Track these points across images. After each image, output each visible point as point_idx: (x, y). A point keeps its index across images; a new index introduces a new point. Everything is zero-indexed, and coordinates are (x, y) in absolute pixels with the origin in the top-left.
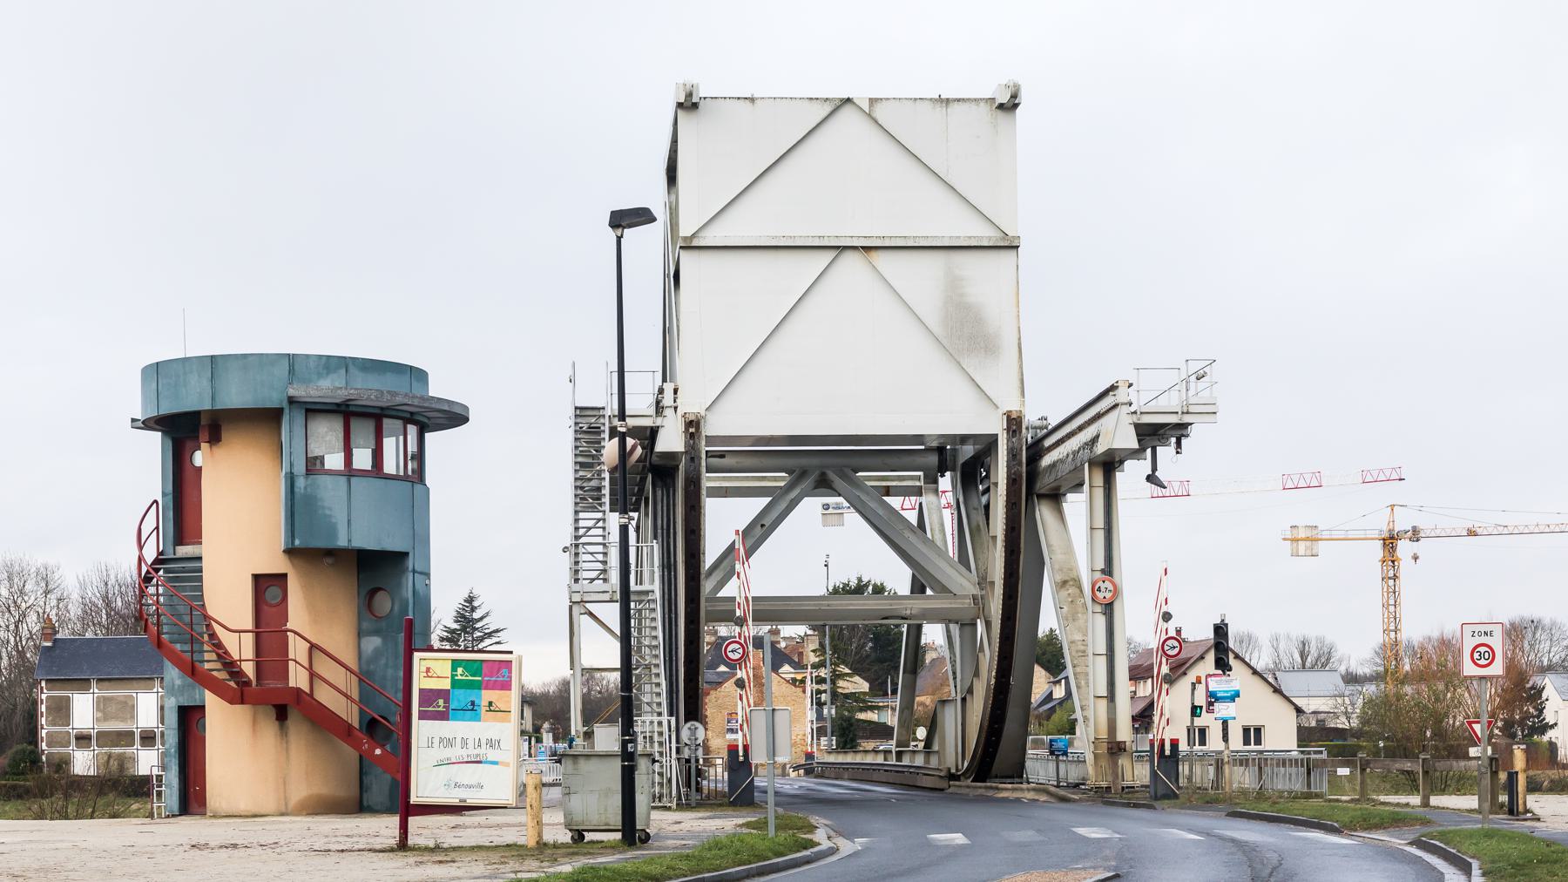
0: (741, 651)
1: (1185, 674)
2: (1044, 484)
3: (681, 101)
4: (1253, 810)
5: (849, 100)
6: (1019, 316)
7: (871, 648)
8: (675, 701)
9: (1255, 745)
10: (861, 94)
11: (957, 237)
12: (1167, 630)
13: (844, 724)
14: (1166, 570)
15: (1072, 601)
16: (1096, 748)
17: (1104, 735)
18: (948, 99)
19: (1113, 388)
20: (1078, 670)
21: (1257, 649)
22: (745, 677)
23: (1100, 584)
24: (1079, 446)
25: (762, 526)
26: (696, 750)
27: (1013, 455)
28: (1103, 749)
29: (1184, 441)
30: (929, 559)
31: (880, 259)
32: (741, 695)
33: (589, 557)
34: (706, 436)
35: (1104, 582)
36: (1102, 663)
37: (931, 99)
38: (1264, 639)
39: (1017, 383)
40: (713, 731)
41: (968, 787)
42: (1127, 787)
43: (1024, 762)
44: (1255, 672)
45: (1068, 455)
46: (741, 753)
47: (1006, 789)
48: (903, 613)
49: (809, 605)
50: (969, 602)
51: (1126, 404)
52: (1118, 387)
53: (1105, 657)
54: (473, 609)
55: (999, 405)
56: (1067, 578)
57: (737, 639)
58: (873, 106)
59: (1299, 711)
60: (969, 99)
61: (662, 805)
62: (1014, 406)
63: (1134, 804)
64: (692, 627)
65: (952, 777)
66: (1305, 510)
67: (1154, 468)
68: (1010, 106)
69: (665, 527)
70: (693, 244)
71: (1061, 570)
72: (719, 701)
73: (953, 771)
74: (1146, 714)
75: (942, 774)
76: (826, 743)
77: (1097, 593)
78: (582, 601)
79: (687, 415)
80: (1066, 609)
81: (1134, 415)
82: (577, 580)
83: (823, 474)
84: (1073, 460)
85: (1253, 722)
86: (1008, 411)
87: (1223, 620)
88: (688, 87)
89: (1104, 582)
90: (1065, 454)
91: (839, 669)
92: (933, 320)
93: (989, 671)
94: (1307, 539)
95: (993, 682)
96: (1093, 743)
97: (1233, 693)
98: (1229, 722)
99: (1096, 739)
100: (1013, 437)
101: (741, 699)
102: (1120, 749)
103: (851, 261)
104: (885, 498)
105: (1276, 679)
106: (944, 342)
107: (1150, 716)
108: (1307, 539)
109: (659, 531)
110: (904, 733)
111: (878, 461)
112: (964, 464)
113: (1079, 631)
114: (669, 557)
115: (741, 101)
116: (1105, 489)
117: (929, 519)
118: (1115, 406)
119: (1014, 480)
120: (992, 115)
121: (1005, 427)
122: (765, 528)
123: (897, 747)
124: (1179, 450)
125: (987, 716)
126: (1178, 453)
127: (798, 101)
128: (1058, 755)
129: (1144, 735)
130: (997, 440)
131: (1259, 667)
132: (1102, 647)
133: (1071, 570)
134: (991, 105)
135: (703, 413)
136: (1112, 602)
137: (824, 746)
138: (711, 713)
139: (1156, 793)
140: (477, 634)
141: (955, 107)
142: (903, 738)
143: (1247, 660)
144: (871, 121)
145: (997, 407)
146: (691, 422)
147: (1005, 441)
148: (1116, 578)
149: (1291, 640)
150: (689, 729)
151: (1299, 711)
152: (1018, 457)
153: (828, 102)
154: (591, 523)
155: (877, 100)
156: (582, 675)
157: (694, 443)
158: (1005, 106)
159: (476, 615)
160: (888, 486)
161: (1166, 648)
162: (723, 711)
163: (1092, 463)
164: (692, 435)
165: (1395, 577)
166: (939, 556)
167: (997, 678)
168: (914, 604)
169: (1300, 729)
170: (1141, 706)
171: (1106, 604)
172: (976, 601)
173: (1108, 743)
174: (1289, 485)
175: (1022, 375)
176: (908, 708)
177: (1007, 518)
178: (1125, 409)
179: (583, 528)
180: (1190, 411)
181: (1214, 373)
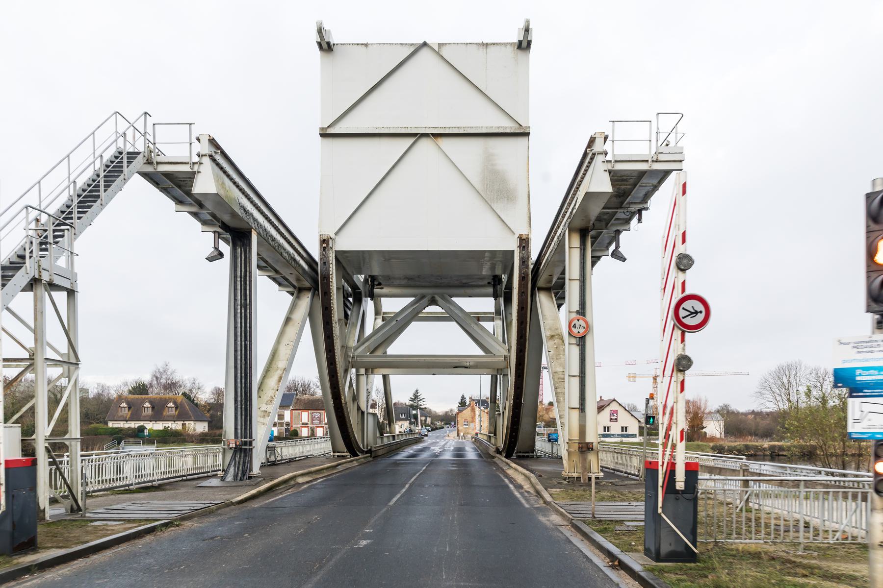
1: (603, 410)
5: (425, 44)
6: (528, 177)
12: (683, 283)
15: (556, 348)
16: (569, 447)
17: (576, 436)
18: (487, 43)
20: (558, 390)
23: (576, 322)
27: (523, 262)
28: (575, 448)
30: (485, 339)
31: (444, 143)
35: (578, 320)
36: (576, 382)
37: (477, 43)
39: (527, 219)
43: (534, 442)
50: (502, 359)
52: (595, 138)
53: (579, 249)
54: (417, 393)
55: (515, 232)
56: (554, 334)
58: (440, 48)
59: (639, 421)
62: (524, 231)
64: (332, 367)
66: (632, 370)
68: (524, 45)
69: (243, 276)
71: (550, 329)
77: (573, 329)
79: (322, 236)
80: (552, 352)
81: (609, 164)
83: (433, 297)
85: (624, 425)
86: (520, 235)
89: (578, 320)
94: (633, 377)
95: (512, 402)
96: (567, 443)
99: (569, 440)
100: (523, 250)
108: (633, 377)
109: (239, 279)
113: (560, 366)
114: (245, 299)
115: (360, 46)
119: (523, 278)
121: (518, 245)
125: (510, 421)
127: (394, 46)
128: (552, 442)
132: (576, 371)
133: (557, 329)
135: (333, 236)
136: (585, 336)
140: (418, 399)
141: (491, 49)
145: (514, 234)
146: (324, 240)
148: (588, 318)
151: (639, 421)
152: (526, 263)
153: (413, 46)
159: (418, 395)
160: (479, 317)
161: (682, 313)
165: (656, 387)
169: (640, 427)
171: (579, 338)
173: (579, 443)
175: (530, 214)
177: (519, 303)
178: (599, 159)
180: (660, 159)
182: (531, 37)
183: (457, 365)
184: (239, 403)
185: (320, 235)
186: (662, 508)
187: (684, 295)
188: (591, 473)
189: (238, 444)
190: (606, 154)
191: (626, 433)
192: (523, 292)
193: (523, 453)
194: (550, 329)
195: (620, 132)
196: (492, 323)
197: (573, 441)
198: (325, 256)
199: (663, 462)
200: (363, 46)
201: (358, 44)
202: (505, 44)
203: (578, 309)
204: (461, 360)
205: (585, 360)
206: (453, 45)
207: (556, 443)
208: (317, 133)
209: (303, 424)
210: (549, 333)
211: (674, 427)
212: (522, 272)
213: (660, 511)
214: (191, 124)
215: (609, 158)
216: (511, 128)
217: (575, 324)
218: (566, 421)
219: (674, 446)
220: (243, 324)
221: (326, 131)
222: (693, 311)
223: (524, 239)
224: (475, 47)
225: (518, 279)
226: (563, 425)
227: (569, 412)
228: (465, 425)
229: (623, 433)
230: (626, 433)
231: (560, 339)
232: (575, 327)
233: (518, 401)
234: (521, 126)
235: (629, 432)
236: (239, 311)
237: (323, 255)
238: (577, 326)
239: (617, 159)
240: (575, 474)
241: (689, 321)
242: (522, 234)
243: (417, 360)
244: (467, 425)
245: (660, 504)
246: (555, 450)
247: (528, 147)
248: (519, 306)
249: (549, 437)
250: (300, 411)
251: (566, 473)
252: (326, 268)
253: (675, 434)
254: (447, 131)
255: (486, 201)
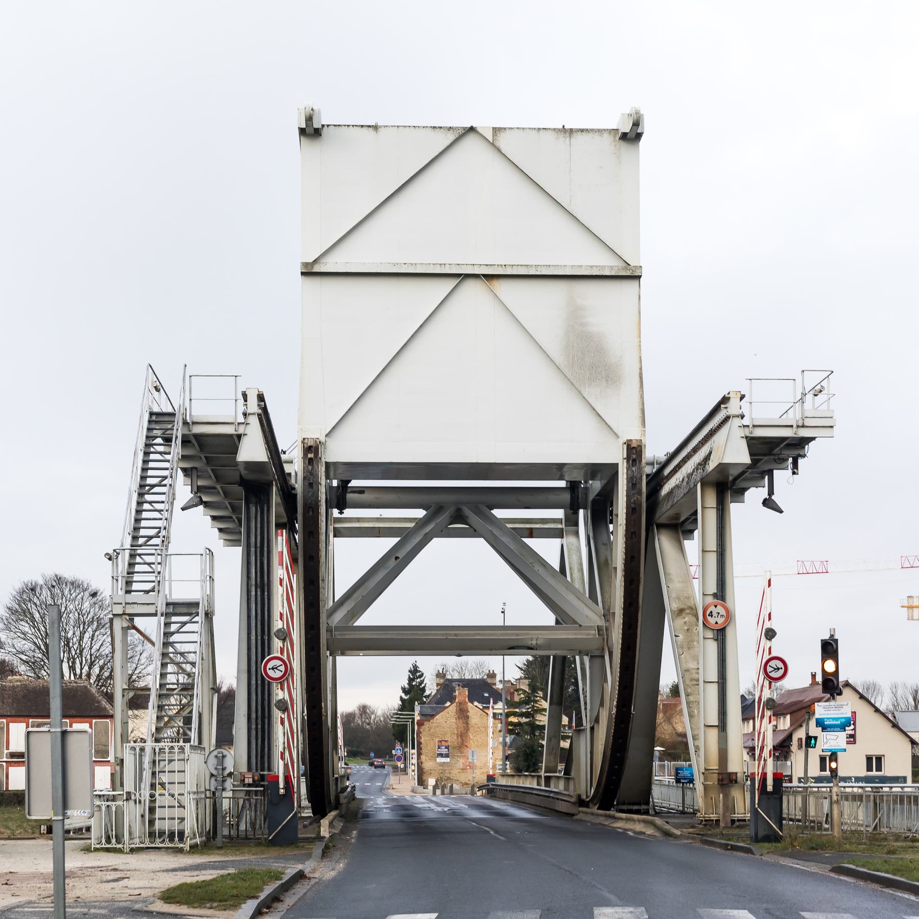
0: (282, 668)
2: (664, 513)
3: (304, 126)
4: (863, 866)
5: (472, 129)
6: (640, 346)
7: (573, 690)
8: (266, 727)
9: (876, 771)
10: (484, 124)
11: (579, 266)
12: (770, 649)
13: (527, 750)
14: (769, 581)
15: (688, 630)
16: (706, 779)
17: (714, 766)
18: (571, 130)
19: (725, 400)
20: (691, 698)
21: (880, 695)
22: (287, 697)
23: (712, 608)
24: (693, 467)
25: (397, 558)
26: (224, 781)
28: (713, 780)
29: (801, 461)
31: (504, 289)
32: (282, 719)
33: (146, 568)
34: (326, 463)
35: (716, 606)
36: (713, 690)
37: (555, 129)
38: (885, 685)
39: (638, 413)
40: (426, 755)
41: (592, 814)
42: (738, 820)
44: (877, 710)
45: (683, 479)
46: (281, 785)
47: (621, 819)
48: (529, 643)
49: (437, 634)
51: (738, 416)
52: (729, 398)
55: (619, 434)
57: (279, 655)
60: (592, 130)
61: (173, 845)
62: (634, 435)
63: (732, 846)
64: (312, 653)
65: (581, 803)
67: (771, 492)
69: (259, 545)
70: (314, 270)
71: (678, 598)
72: (432, 730)
73: (584, 797)
74: (785, 744)
75: (573, 800)
76: (501, 767)
77: (709, 618)
78: (124, 614)
79: (306, 441)
80: (681, 637)
81: (746, 429)
82: (128, 592)
83: (459, 510)
84: (687, 483)
87: (832, 636)
88: (309, 110)
89: (716, 606)
90: (681, 479)
91: (537, 705)
92: (555, 349)
93: (611, 700)
95: (614, 711)
96: (703, 773)
97: (844, 720)
98: (839, 754)
99: (706, 769)
100: (633, 466)
101: (282, 723)
102: (731, 781)
103: (473, 291)
104: (526, 540)
105: (895, 717)
106: (569, 375)
107: (789, 746)
109: (253, 549)
110: (552, 759)
111: (512, 498)
112: (594, 501)
115: (365, 129)
116: (718, 509)
117: (569, 558)
118: (727, 418)
119: (634, 509)
120: (615, 146)
121: (625, 456)
122: (398, 560)
123: (545, 772)
124: (795, 471)
125: (610, 744)
126: (794, 473)
128: (683, 783)
129: (784, 762)
130: (617, 472)
131: (882, 708)
132: (713, 675)
133: (688, 598)
134: (615, 137)
135: (323, 439)
136: (725, 628)
137: (499, 769)
138: (424, 740)
139: (756, 834)
141: (578, 138)
142: (552, 764)
143: (873, 701)
144: (497, 151)
146: (310, 447)
147: (625, 470)
148: (729, 603)
149: (907, 688)
150: (216, 757)
152: (638, 486)
153: (451, 131)
154: (152, 532)
155: (500, 129)
156: (123, 696)
157: (313, 469)
158: (628, 136)
160: (532, 529)
161: (769, 669)
162: (435, 739)
163: (705, 483)
164: (311, 460)
166: (567, 588)
167: (618, 707)
168: (540, 634)
170: (781, 737)
171: (718, 630)
172: (601, 632)
173: (719, 774)
174: (907, 565)
175: (643, 404)
176: (555, 737)
177: (626, 548)
178: (736, 422)
179: (142, 537)
180: (806, 424)
181: (832, 386)
182: (643, 128)
183: (513, 644)
184: (253, 721)
185: (304, 439)
186: (758, 804)
187: (770, 656)
188: (735, 814)
189: (256, 778)
190: (742, 417)
191: (879, 773)
192: (635, 532)
193: (630, 804)
194: (678, 598)
195: (755, 392)
196: (556, 543)
197: (712, 771)
198: (311, 474)
199: (758, 773)
200: (370, 129)
201: (362, 126)
202: (600, 131)
203: (715, 591)
204: (522, 634)
205: (725, 660)
206: (516, 131)
207: (691, 785)
208: (299, 270)
209: (13, 755)
210: (675, 606)
211: (765, 747)
212: (632, 501)
213: (757, 806)
214: (236, 376)
215: (746, 421)
216: (612, 268)
217: (711, 612)
218: (701, 743)
219: (765, 760)
220: (259, 612)
221: (312, 267)
222: (776, 667)
223: (634, 448)
224: (551, 136)
225: (625, 511)
226: (697, 749)
227: (705, 732)
228: (441, 755)
229: (870, 773)
230: (879, 773)
231: (693, 615)
232: (712, 616)
233: (624, 709)
234: (629, 265)
235: (889, 770)
236: (253, 593)
237: (308, 471)
238: (715, 614)
239: (756, 424)
240: (714, 815)
241: (774, 675)
242: (631, 440)
243: (442, 635)
244: (447, 756)
245: (757, 802)
246: (688, 801)
247: (639, 296)
248: (626, 554)
249: (677, 774)
250: (5, 721)
251: (702, 814)
252: (313, 493)
253: (766, 753)
254: (509, 272)
255: (572, 384)
